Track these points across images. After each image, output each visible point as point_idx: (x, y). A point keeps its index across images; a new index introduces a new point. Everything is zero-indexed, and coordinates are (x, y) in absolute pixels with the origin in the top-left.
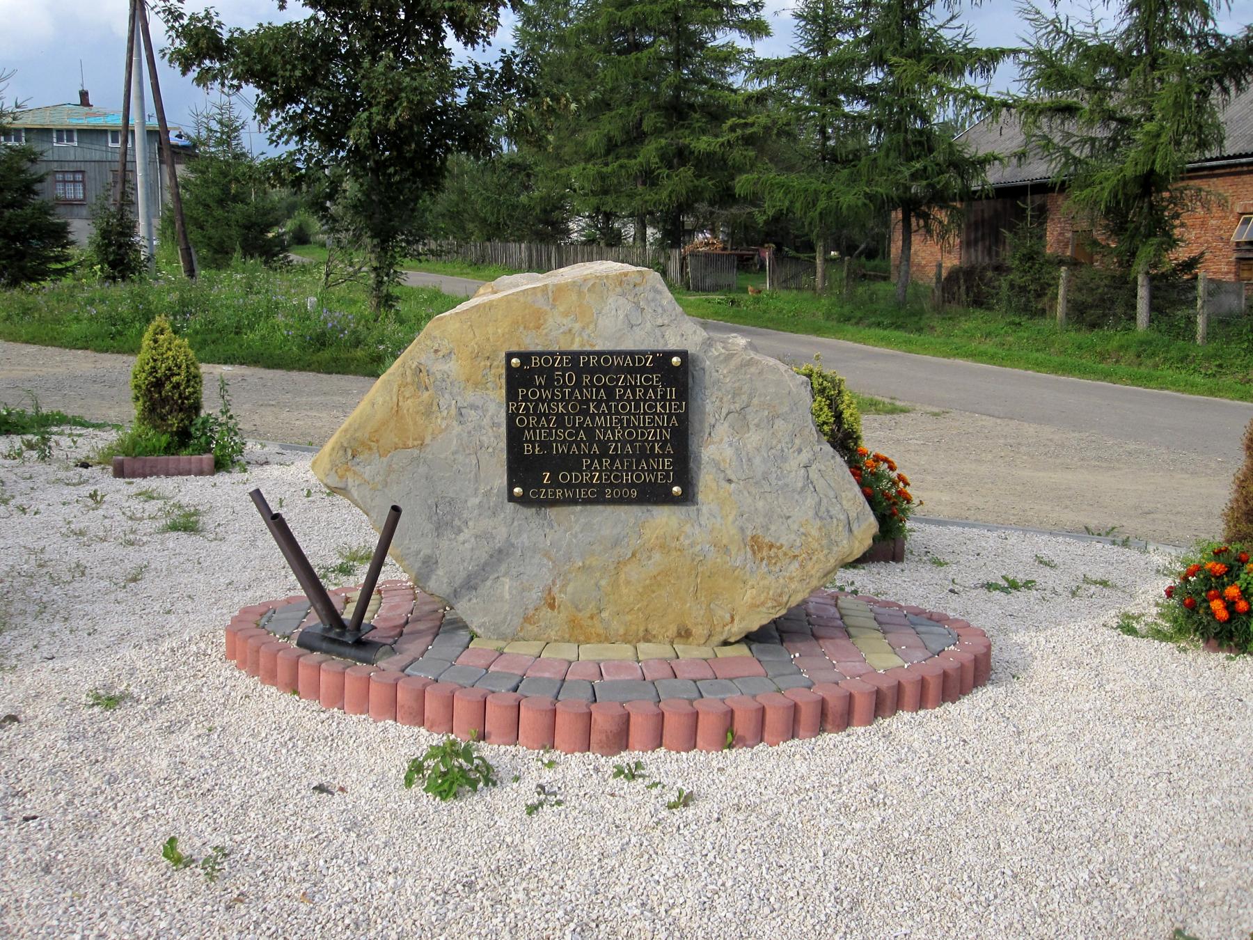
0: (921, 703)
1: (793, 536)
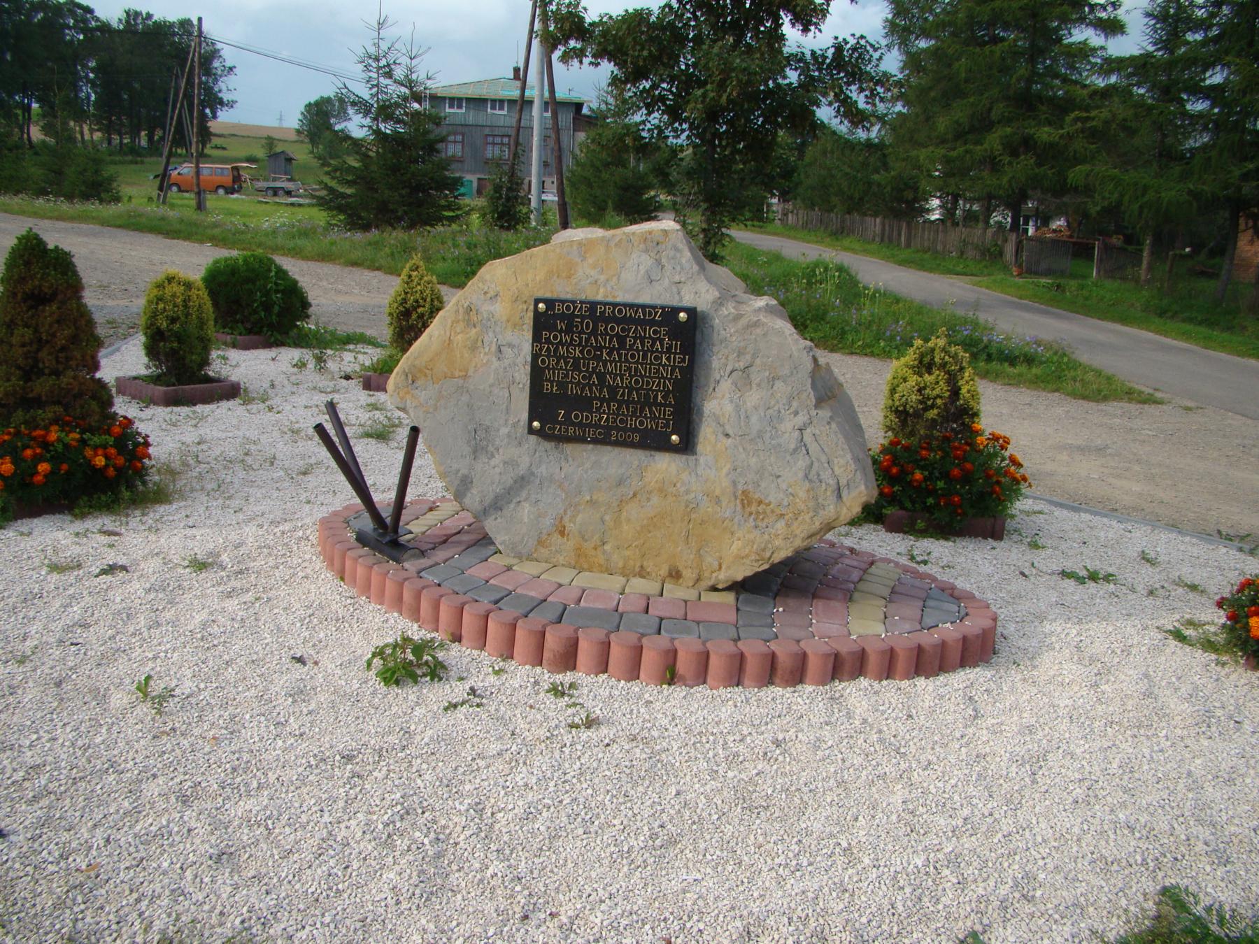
0: (888, 671)
1: (781, 495)
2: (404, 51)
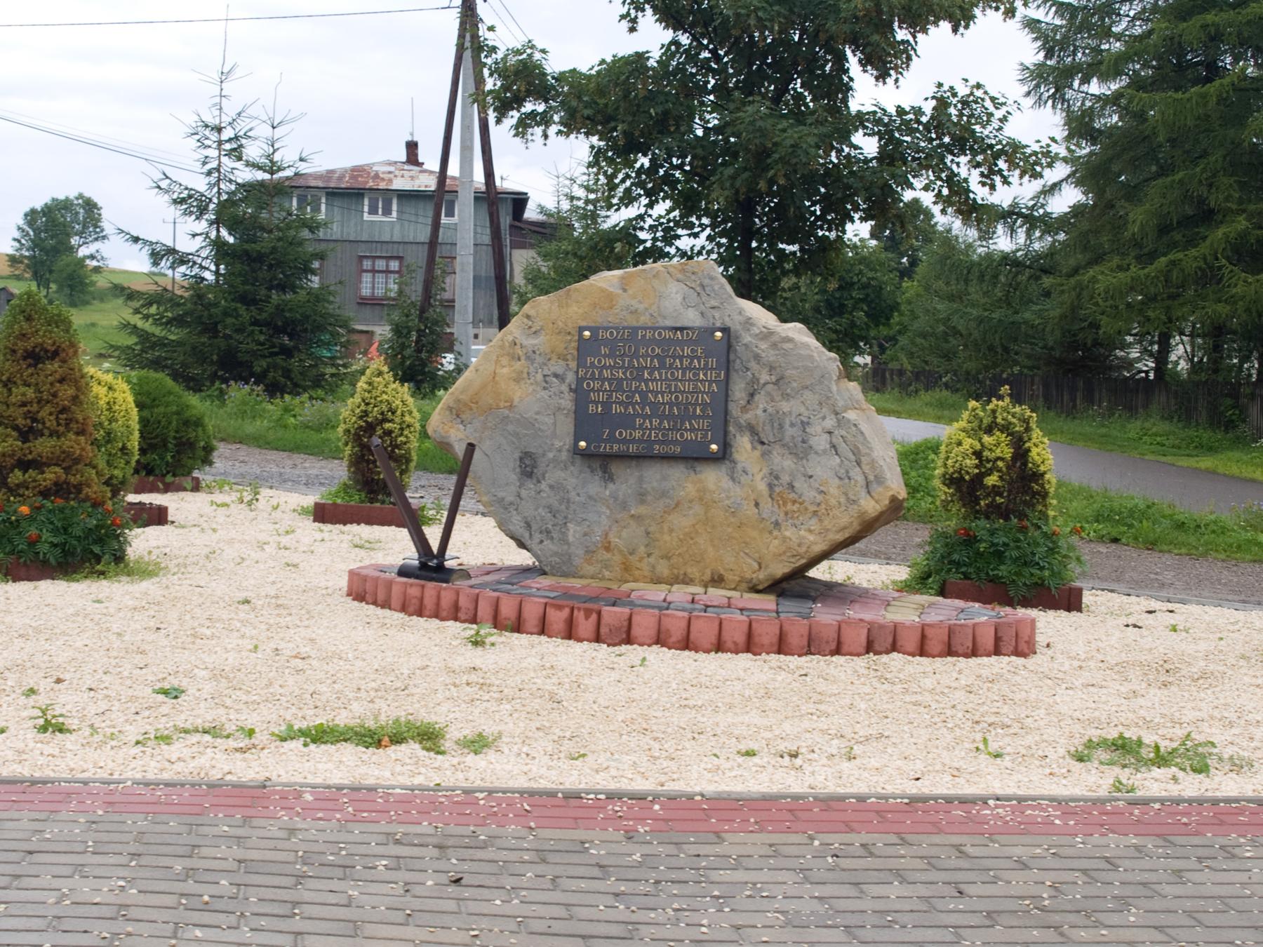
2: (265, 118)
